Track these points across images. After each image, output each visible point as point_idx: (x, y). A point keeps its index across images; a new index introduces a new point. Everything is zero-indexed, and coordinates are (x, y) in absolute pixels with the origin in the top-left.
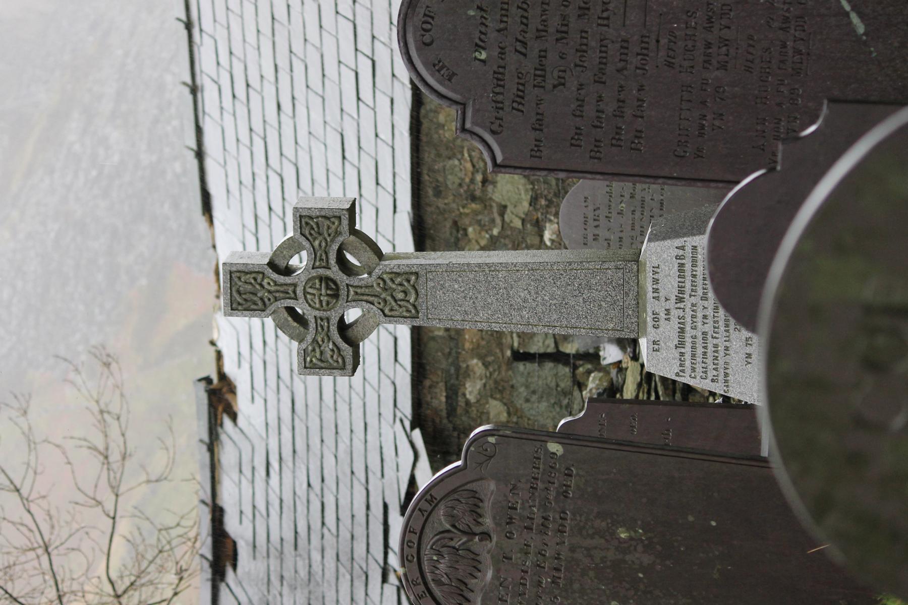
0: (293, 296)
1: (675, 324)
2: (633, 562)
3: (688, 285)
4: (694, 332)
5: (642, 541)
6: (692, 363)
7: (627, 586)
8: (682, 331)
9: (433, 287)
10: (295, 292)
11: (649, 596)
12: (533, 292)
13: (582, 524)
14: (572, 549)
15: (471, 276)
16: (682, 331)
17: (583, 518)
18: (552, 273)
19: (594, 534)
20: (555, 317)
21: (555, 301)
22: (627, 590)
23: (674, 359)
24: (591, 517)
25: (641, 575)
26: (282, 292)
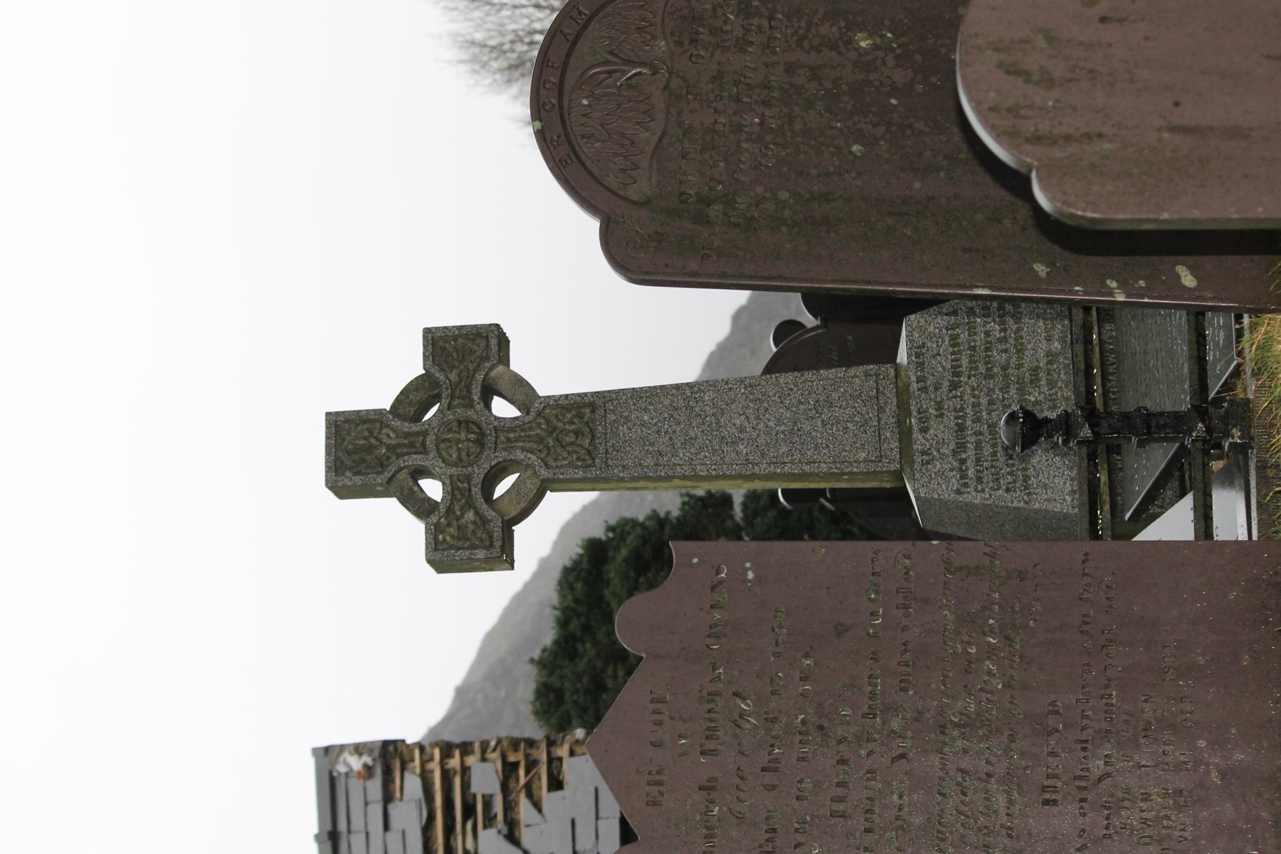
0: (421, 449)
1: (950, 420)
2: (881, 83)
3: (965, 362)
4: (977, 427)
5: (892, 50)
6: (978, 471)
7: (875, 120)
8: (961, 428)
9: (614, 421)
10: (423, 444)
11: (908, 132)
12: (752, 417)
13: (802, 32)
14: (790, 69)
15: (667, 402)
16: (961, 428)
17: (803, 24)
18: (777, 389)
19: (821, 44)
20: (784, 449)
21: (783, 428)
22: (874, 126)
23: (951, 470)
24: (816, 20)
25: (894, 102)
26: (405, 445)
